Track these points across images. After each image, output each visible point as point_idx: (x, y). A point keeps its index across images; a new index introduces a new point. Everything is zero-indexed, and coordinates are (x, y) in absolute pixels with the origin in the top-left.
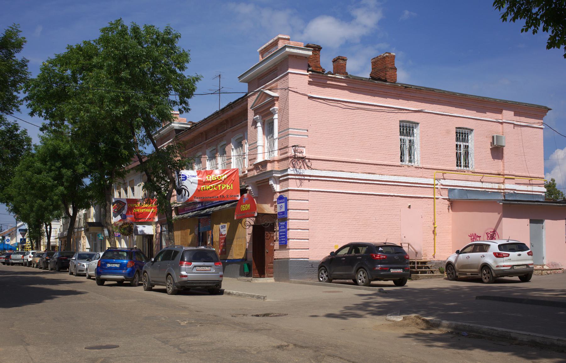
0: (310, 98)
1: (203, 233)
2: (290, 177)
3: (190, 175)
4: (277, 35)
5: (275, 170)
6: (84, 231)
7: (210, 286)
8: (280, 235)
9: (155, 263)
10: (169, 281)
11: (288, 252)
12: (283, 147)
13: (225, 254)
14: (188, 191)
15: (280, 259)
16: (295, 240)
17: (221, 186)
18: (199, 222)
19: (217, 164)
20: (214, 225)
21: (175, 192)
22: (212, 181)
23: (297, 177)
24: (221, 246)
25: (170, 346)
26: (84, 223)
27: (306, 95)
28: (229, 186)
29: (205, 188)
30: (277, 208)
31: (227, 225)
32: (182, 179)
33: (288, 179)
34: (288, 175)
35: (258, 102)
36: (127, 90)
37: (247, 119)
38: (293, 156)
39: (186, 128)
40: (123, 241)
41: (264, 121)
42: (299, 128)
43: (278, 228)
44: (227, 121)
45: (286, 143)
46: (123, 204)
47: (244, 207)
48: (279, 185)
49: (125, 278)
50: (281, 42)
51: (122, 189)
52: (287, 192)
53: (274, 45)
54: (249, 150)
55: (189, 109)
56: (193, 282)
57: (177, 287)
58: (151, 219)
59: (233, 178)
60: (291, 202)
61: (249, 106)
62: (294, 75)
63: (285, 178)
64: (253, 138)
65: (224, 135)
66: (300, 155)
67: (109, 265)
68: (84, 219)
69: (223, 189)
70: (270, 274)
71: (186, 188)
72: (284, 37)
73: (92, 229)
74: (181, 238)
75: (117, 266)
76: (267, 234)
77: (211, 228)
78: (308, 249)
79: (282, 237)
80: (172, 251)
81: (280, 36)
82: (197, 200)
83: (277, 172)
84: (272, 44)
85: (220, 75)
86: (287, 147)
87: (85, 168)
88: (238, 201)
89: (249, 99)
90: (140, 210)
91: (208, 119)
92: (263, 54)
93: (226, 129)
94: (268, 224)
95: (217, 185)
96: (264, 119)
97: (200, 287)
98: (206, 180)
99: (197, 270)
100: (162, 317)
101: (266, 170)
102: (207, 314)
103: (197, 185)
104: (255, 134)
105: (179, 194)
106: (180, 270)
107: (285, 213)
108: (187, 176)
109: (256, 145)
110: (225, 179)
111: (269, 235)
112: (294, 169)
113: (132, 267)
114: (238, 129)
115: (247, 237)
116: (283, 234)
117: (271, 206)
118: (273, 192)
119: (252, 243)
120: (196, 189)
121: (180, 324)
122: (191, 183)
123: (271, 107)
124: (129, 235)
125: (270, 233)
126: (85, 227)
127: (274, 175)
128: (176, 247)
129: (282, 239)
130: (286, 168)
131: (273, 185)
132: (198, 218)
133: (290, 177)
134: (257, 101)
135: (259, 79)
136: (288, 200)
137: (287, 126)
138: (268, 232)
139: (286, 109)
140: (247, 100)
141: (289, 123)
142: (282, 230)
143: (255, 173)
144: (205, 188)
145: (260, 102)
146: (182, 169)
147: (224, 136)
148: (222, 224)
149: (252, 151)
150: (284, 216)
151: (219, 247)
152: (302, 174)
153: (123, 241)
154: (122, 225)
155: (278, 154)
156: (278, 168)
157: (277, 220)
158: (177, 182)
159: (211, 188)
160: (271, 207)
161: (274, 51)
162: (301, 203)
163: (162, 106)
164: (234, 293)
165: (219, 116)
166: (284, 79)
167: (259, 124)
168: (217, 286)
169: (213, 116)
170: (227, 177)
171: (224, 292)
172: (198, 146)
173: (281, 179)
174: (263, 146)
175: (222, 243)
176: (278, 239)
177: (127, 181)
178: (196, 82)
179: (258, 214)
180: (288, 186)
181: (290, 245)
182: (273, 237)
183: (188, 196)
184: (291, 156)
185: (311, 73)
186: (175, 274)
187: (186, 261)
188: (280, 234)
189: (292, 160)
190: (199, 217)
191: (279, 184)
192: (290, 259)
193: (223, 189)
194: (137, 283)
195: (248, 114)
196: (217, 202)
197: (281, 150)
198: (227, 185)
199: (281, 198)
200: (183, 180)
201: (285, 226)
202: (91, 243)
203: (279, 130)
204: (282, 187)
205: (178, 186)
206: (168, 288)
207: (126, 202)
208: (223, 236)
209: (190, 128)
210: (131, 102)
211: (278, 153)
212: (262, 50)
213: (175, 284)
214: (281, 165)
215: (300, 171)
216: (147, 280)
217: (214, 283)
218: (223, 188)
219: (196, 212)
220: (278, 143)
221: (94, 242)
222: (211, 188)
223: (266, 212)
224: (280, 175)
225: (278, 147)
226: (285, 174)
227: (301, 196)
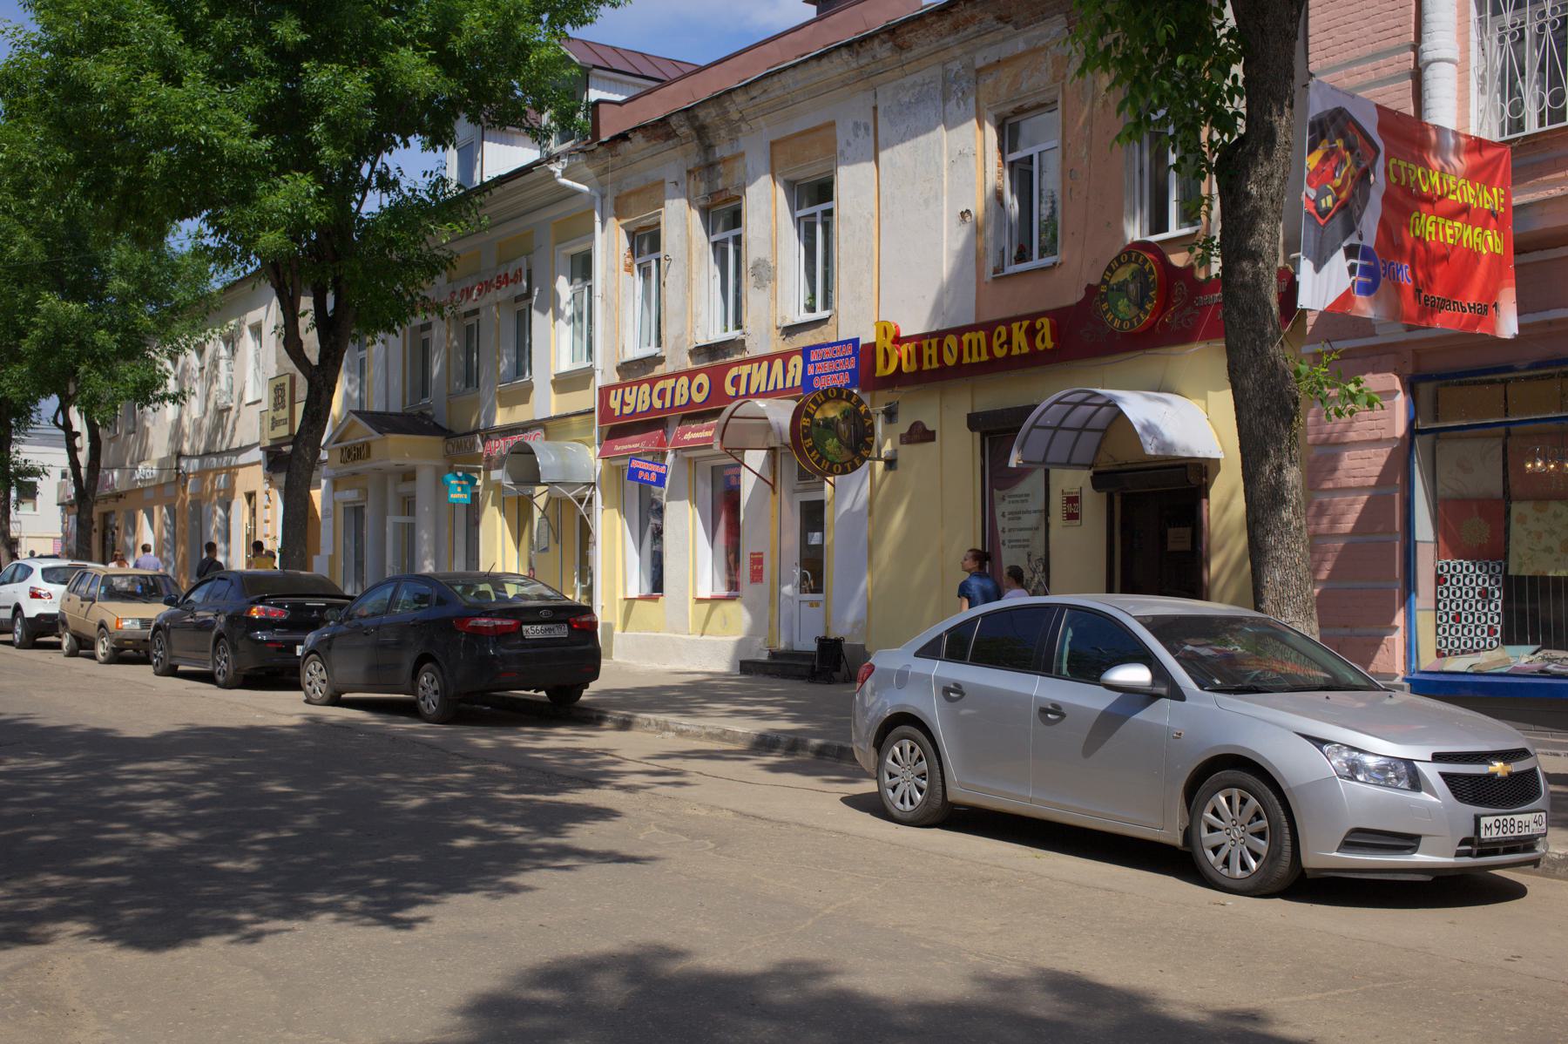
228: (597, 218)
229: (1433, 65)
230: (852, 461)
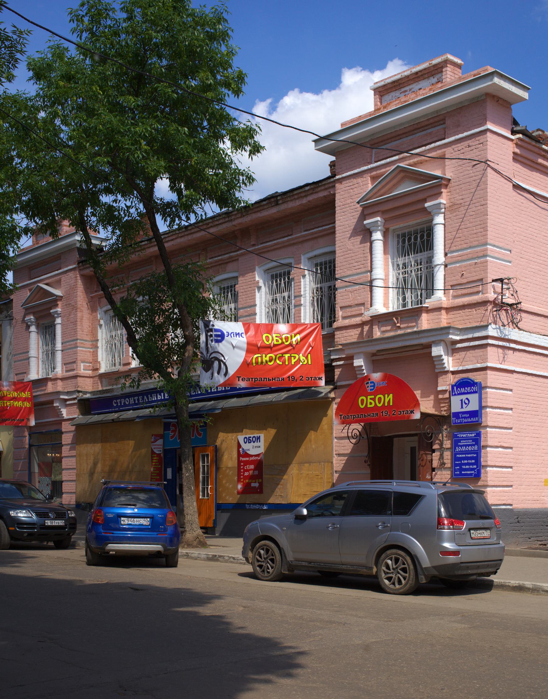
0: (517, 187)
2: (490, 341)
4: (445, 53)
17: (290, 358)
22: (275, 345)
23: (501, 343)
27: (509, 180)
28: (304, 358)
29: (260, 359)
34: (487, 337)
42: (500, 245)
53: (426, 76)
58: (23, 420)
71: (223, 358)
78: (511, 486)
81: (451, 57)
82: (242, 384)
84: (420, 74)
95: (282, 354)
96: (387, 226)
98: (263, 344)
101: (416, 326)
103: (243, 354)
120: (241, 360)
122: (234, 347)
129: (463, 467)
131: (445, 357)
133: (490, 341)
152: (507, 337)
159: (270, 361)
162: (503, 395)
170: (302, 339)
179: (422, 414)
185: (520, 136)
193: (293, 363)
198: (301, 355)
201: (477, 440)
205: (205, 353)
218: (293, 361)
224: (458, 338)
229: (377, 280)
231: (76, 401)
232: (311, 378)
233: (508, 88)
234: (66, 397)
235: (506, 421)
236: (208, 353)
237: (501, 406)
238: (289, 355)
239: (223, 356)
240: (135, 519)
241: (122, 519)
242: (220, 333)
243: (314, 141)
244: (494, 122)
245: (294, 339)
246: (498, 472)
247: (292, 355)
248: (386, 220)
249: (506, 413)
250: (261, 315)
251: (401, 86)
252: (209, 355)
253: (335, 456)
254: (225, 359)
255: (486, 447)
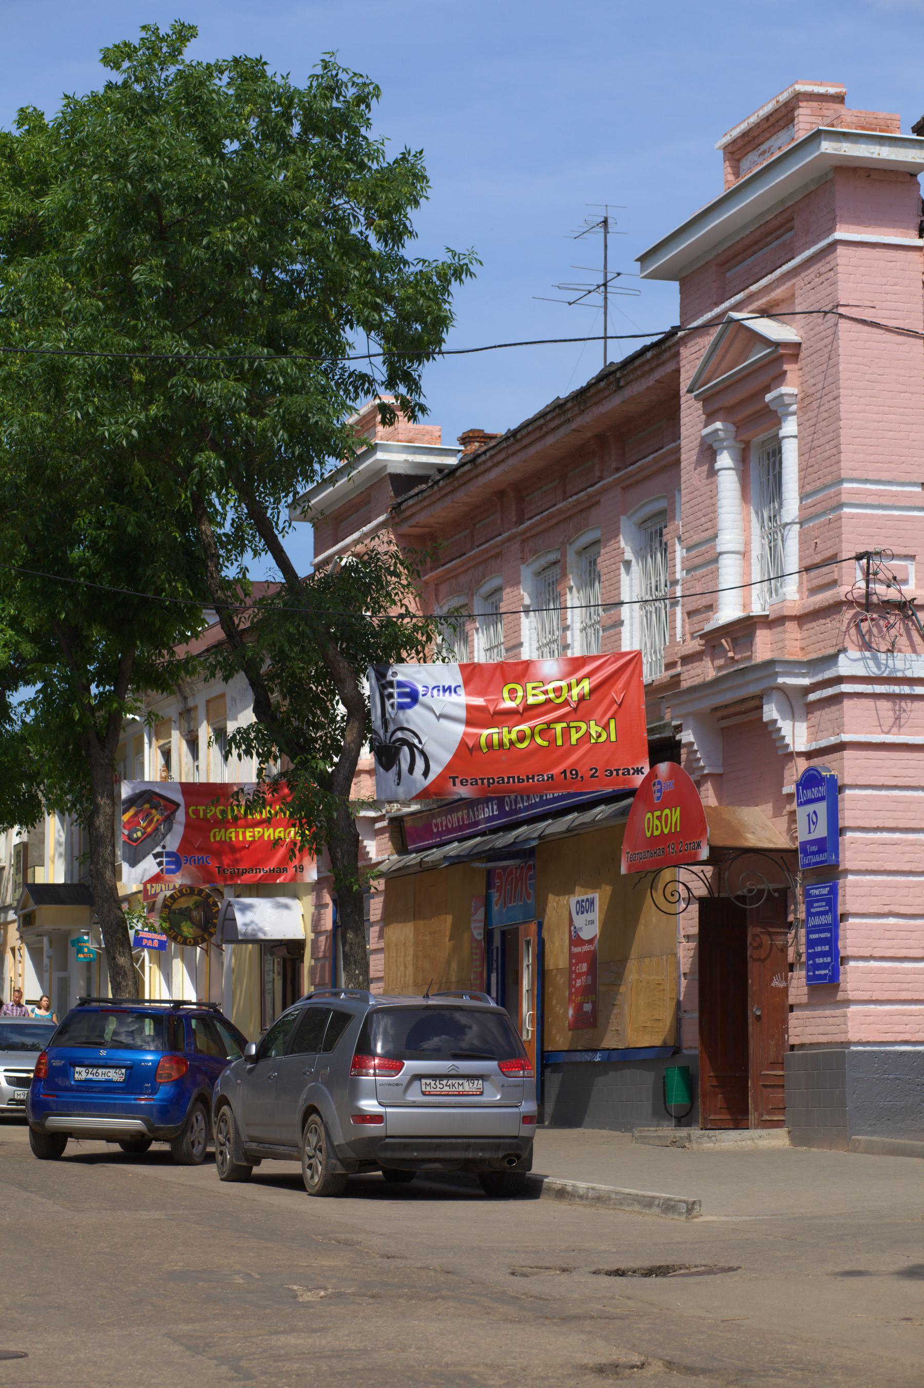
1: (503, 933)
2: (846, 688)
3: (432, 684)
5: (787, 657)
6: (16, 925)
7: (482, 1160)
8: (810, 944)
9: (262, 1064)
10: (313, 1139)
11: (845, 1016)
12: (818, 559)
13: (594, 1025)
14: (422, 753)
15: (812, 1045)
16: (873, 964)
17: (566, 732)
18: (489, 885)
19: (566, 628)
20: (551, 897)
21: (366, 757)
24: (577, 989)
25: (210, 1359)
26: (16, 886)
28: (599, 729)
29: (496, 737)
30: (795, 821)
31: (599, 897)
32: (396, 700)
33: (838, 699)
34: (840, 680)
35: (719, 364)
36: (156, 337)
37: (677, 436)
38: (860, 597)
39: (440, 469)
40: (179, 967)
41: (747, 443)
42: (884, 476)
43: (802, 915)
44: (601, 440)
45: (829, 543)
46: (166, 809)
47: (657, 822)
48: (805, 725)
49: (149, 1130)
50: (809, 112)
51: (176, 735)
52: (837, 755)
53: (782, 123)
54: (688, 571)
55: (423, 409)
56: (409, 1142)
57: (344, 1162)
59: (616, 693)
60: (854, 799)
61: (685, 381)
62: (862, 251)
63: (829, 692)
64: (703, 520)
65: (593, 503)
66: (891, 594)
67: (81, 1074)
68: (17, 871)
69: (574, 741)
70: (768, 1113)
71: (416, 741)
72: (821, 90)
73: (49, 915)
74: (416, 957)
75: (116, 1075)
76: (754, 936)
77: (538, 916)
79: (818, 949)
80: (329, 1011)
81: (801, 88)
82: (463, 791)
83: (794, 666)
84: (772, 120)
85: (605, 222)
86: (833, 560)
87: (17, 643)
88: (632, 793)
89: (684, 352)
90: (240, 831)
91: (524, 432)
92: (739, 160)
93: (598, 474)
94: (761, 892)
95: (548, 723)
96: (744, 437)
97: (437, 1165)
99: (424, 1093)
100: (238, 1272)
101: (750, 658)
102: (419, 1265)
104: (708, 502)
105: (387, 768)
106: (354, 1093)
107: (829, 845)
108: (421, 689)
109: (714, 548)
110: (582, 698)
111: (766, 939)
112: (867, 654)
113: (178, 1083)
114: (544, 531)
115: (681, 953)
116: (823, 935)
117: (777, 813)
118: (780, 752)
119: (697, 977)
121: (295, 1297)
123: (768, 389)
124: (204, 940)
125: (770, 934)
126: (19, 906)
127: (780, 680)
128: (343, 996)
129: (820, 961)
130: (832, 651)
131: (780, 724)
132: (483, 865)
133: (846, 688)
134: (715, 358)
135: (721, 265)
136: (841, 789)
137: (835, 468)
138: (759, 930)
139: (830, 397)
140: (678, 354)
141: (843, 456)
142: (816, 921)
143: (708, 670)
144: (496, 738)
145: (729, 357)
146: (401, 660)
147: (590, 507)
148: (580, 895)
149: (698, 573)
150: (822, 857)
151: (570, 994)
152: (899, 675)
153: (179, 967)
154: (172, 896)
155: (800, 591)
156: (802, 649)
157: (800, 875)
158: (376, 715)
159: (521, 739)
160: (775, 816)
161: (780, 144)
162: (895, 800)
163: (299, 399)
164: (581, 1192)
165: (568, 421)
166: (820, 267)
167: (725, 460)
168: (511, 1162)
169: (542, 421)
170: (592, 691)
171: (544, 1186)
172: (487, 550)
173: (812, 697)
174: (745, 554)
175: (579, 976)
176: (804, 959)
177: (199, 700)
178: (454, 286)
179: (713, 849)
180: (841, 729)
181: (849, 986)
182: (784, 950)
183: (426, 774)
184: (850, 597)
186: (334, 1107)
187: (381, 1057)
188: (813, 936)
189: (856, 615)
190: (489, 861)
191: (807, 720)
192: (853, 1048)
193: (574, 741)
194: (197, 1150)
195: (683, 414)
196: (555, 800)
197: (813, 573)
198: (592, 723)
199: (810, 780)
200: (402, 707)
201: (831, 900)
202: (46, 976)
203: (802, 487)
204: (815, 730)
205: (381, 732)
206: (310, 1166)
207: (178, 798)
208: (586, 948)
209: (453, 470)
210: (172, 386)
211: (801, 583)
212: (734, 142)
213: (333, 1150)
214: (814, 638)
215: (890, 662)
216: (232, 1136)
217: (498, 1147)
218: (574, 737)
219: (478, 839)
220: (802, 543)
221: (57, 975)
222: (521, 739)
223: (753, 840)
224: (806, 681)
225: (801, 559)
226: (828, 674)
227: (896, 772)
228: (146, 740)
229: (725, 556)
230: (202, 936)
231: (384, 823)
232: (617, 770)
233: (867, 155)
234: (372, 814)
235: (907, 857)
236: (386, 731)
237: (901, 825)
238: (564, 725)
239: (417, 737)
240: (100, 1071)
241: (78, 1069)
242: (408, 690)
243: (637, 260)
244: (859, 220)
245: (575, 691)
246: (882, 971)
247: (572, 724)
248: (739, 426)
249: (906, 841)
250: (632, 625)
251: (757, 142)
252: (389, 734)
253: (682, 940)
254: (420, 742)
255: (844, 917)
